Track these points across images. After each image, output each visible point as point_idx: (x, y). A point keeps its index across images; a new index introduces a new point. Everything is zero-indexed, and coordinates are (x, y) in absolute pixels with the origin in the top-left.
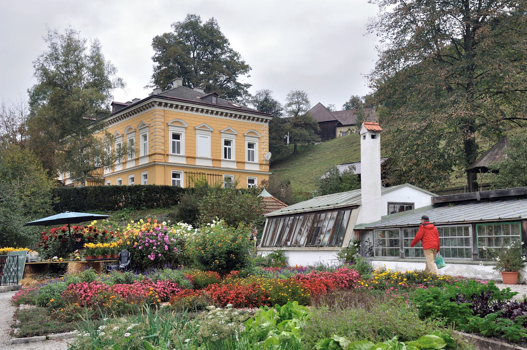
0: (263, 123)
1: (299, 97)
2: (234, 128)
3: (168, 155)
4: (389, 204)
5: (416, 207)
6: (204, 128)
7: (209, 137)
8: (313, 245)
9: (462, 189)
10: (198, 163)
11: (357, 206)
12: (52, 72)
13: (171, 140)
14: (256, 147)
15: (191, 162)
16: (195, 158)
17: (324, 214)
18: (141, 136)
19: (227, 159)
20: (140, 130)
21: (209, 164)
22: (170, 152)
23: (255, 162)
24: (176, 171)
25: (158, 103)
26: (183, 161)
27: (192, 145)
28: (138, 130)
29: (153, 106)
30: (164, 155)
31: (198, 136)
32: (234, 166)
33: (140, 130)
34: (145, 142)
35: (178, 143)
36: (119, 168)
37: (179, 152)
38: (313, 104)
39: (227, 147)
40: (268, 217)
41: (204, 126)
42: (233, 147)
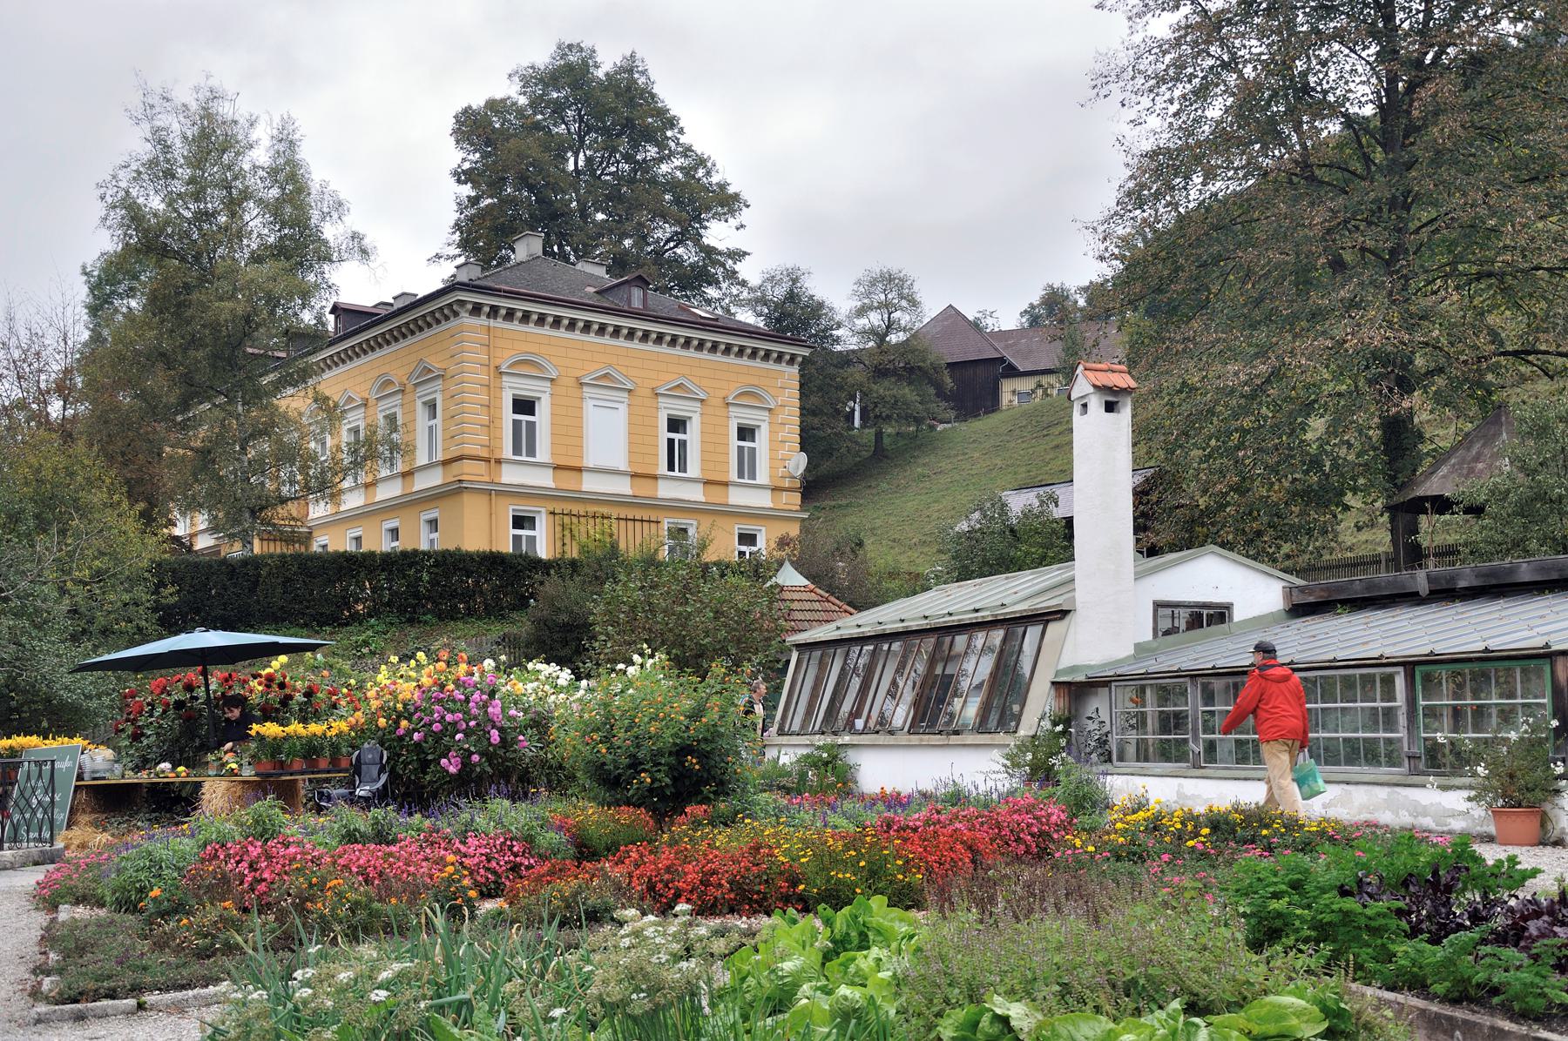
0: (783, 367)
1: (891, 288)
2: (696, 380)
3: (499, 462)
4: (1158, 605)
5: (1238, 615)
6: (606, 381)
7: (623, 408)
8: (932, 729)
9: (1375, 561)
10: (590, 484)
11: (1062, 614)
12: (155, 215)
13: (508, 416)
14: (763, 437)
15: (568, 482)
16: (579, 470)
17: (965, 637)
18: (419, 403)
19: (676, 473)
20: (416, 385)
21: (623, 487)
22: (507, 451)
23: (758, 482)
24: (525, 508)
25: (470, 307)
26: (545, 479)
27: (570, 430)
28: (409, 387)
29: (456, 314)
30: (488, 460)
31: (589, 405)
32: (695, 494)
33: (416, 385)
34: (432, 422)
35: (531, 426)
36: (353, 501)
37: (531, 451)
38: (931, 308)
39: (677, 436)
40: (799, 646)
41: (606, 376)
42: (693, 436)
